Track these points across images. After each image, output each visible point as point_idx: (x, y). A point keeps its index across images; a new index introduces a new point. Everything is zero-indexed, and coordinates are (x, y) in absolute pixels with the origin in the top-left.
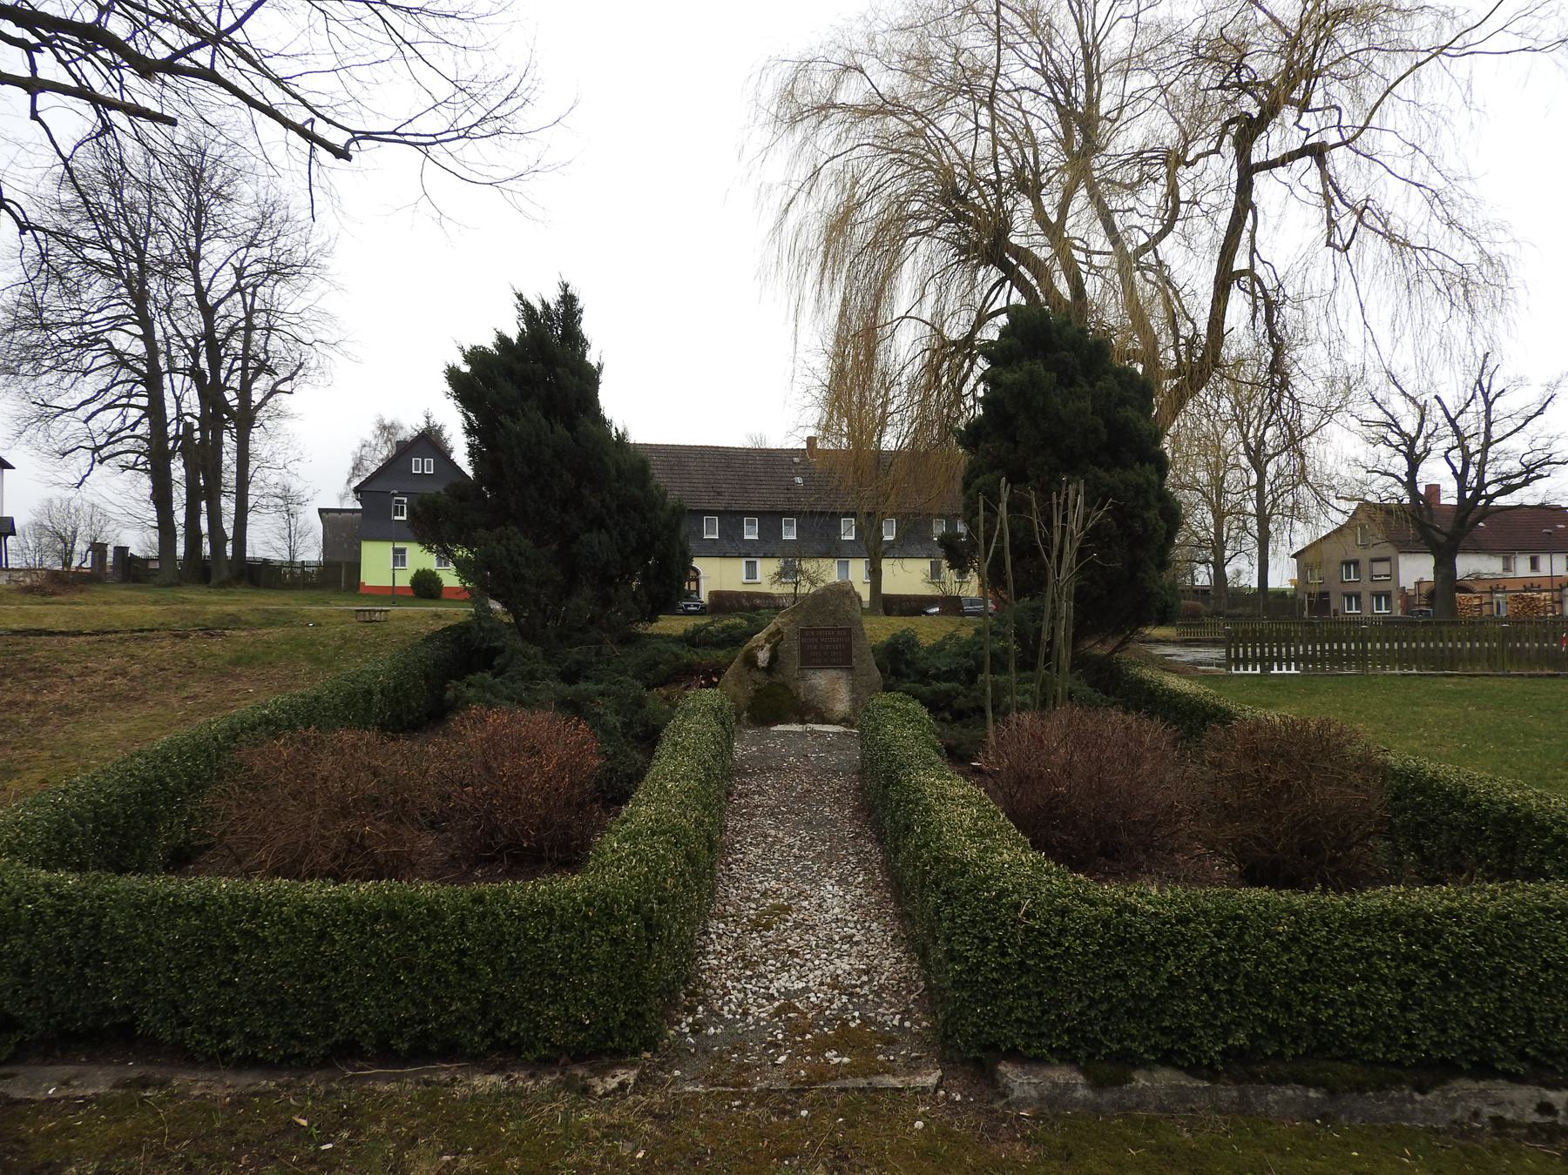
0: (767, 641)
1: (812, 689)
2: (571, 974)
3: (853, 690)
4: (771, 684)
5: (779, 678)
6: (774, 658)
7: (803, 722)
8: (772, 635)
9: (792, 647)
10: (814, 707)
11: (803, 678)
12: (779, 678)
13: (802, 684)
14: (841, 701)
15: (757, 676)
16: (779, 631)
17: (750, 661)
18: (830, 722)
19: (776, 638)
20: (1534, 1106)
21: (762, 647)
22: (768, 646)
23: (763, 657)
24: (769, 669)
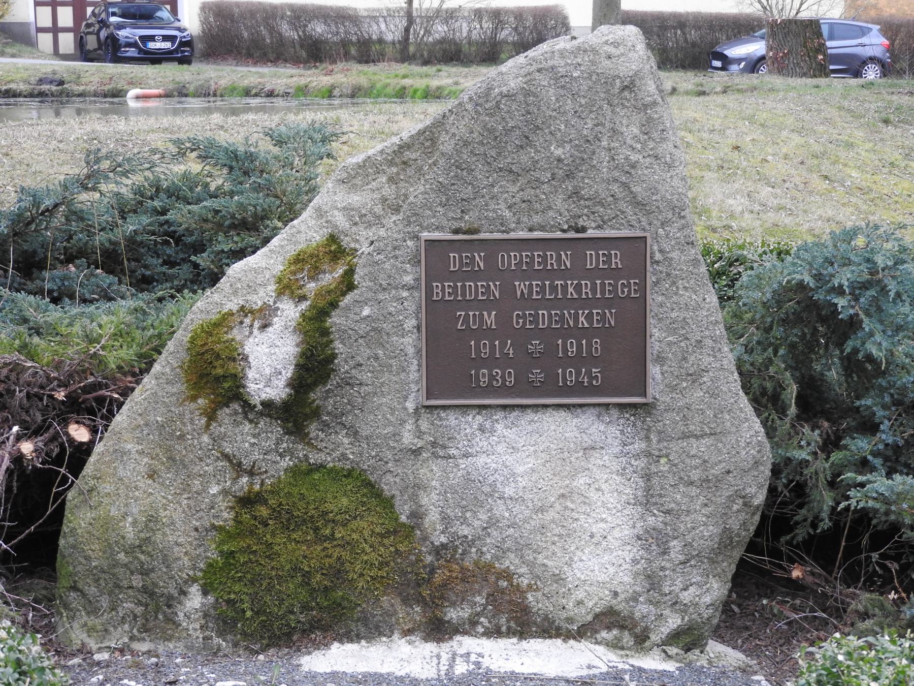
0: (287, 287)
1: (475, 493)
2: (153, 560)
3: (648, 500)
4: (303, 472)
5: (334, 447)
6: (314, 366)
7: (438, 630)
8: (307, 262)
9: (387, 326)
10: (486, 570)
11: (438, 448)
12: (334, 447)
13: (432, 472)
14: (597, 541)
15: (249, 440)
16: (335, 249)
17: (215, 377)
18: (550, 629)
19: (327, 280)
20: (674, 85)
21: (264, 317)
22: (290, 311)
23: (269, 360)
24: (294, 413)
